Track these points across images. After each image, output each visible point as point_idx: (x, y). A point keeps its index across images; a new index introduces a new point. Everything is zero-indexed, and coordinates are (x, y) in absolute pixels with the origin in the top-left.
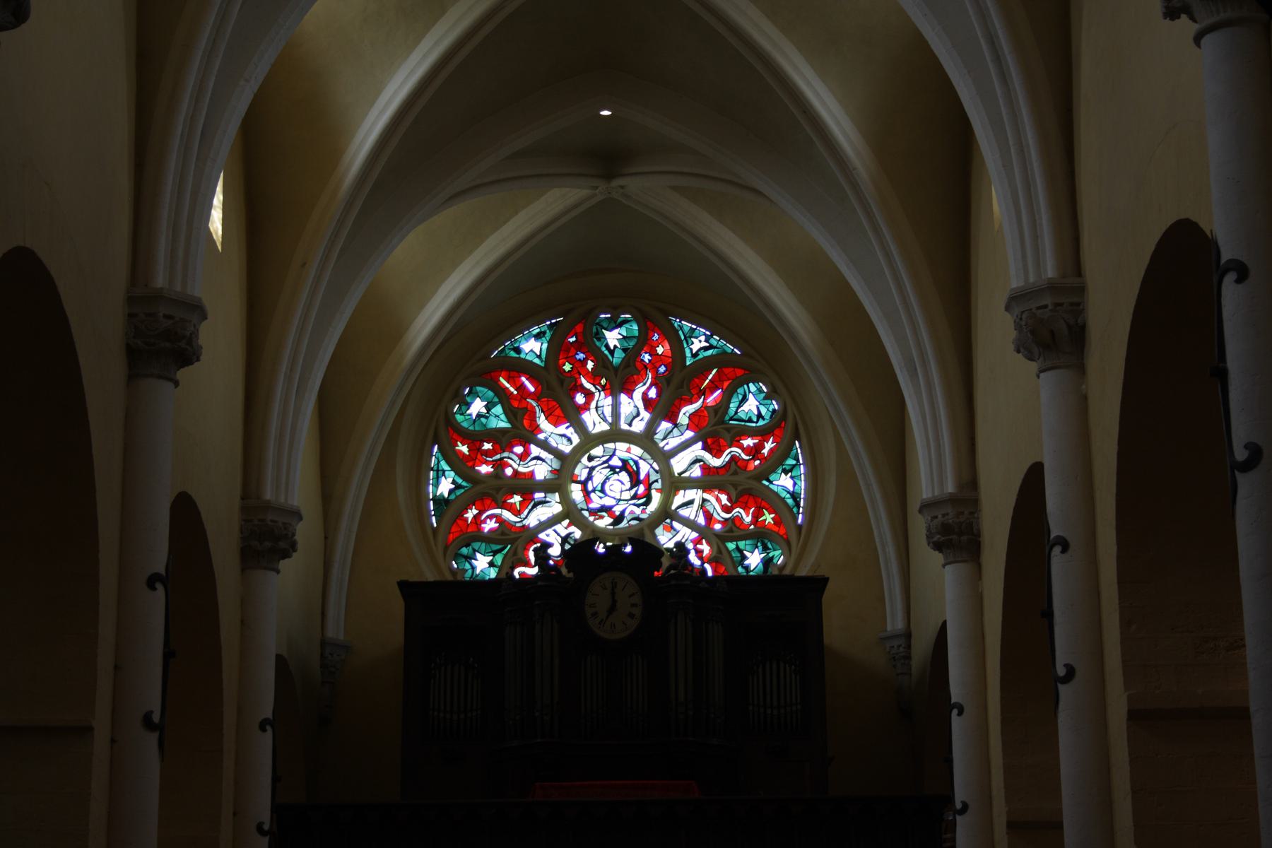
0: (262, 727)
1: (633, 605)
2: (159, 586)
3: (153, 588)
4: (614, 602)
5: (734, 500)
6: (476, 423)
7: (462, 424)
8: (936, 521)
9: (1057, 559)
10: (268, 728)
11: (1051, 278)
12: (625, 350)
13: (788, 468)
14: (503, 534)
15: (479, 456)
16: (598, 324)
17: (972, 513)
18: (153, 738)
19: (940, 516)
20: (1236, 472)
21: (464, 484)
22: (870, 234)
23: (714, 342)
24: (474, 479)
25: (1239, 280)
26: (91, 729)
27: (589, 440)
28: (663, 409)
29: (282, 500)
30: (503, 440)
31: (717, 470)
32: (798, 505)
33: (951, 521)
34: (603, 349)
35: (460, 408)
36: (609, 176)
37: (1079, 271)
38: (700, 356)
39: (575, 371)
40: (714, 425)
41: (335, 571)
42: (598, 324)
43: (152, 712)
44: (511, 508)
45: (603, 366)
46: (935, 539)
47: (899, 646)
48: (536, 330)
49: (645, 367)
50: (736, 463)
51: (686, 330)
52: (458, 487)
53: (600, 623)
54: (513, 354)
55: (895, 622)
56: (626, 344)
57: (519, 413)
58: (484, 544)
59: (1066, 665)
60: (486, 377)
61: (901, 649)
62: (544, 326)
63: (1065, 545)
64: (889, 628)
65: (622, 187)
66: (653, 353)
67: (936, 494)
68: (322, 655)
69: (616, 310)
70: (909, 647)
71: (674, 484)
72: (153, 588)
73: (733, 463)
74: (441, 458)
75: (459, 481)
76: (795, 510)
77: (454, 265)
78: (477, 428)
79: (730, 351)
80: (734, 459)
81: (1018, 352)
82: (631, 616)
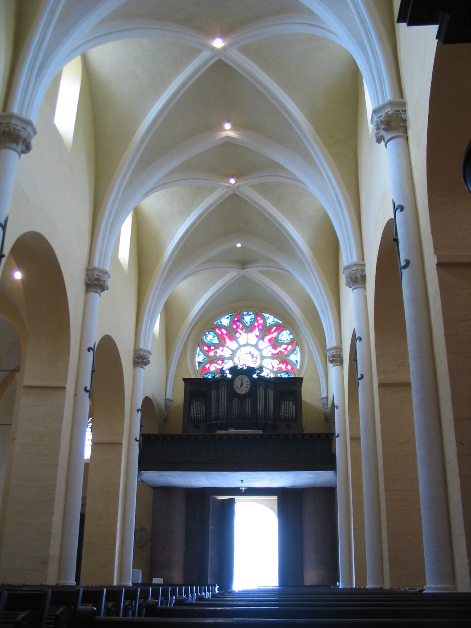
1: (248, 384)
4: (242, 384)
8: (330, 354)
12: (251, 322)
13: (295, 354)
14: (216, 371)
16: (243, 315)
17: (341, 352)
20: (402, 270)
21: (206, 358)
23: (275, 320)
25: (401, 211)
26: (64, 388)
27: (240, 346)
28: (261, 337)
30: (217, 346)
31: (275, 354)
32: (297, 364)
34: (245, 322)
36: (243, 269)
37: (363, 260)
40: (275, 342)
42: (243, 315)
44: (219, 364)
45: (244, 325)
46: (330, 359)
47: (325, 401)
48: (226, 317)
49: (256, 327)
51: (267, 316)
52: (205, 359)
54: (220, 323)
55: (324, 395)
56: (251, 321)
57: (221, 337)
58: (211, 374)
60: (213, 329)
61: (326, 402)
63: (360, 339)
64: (322, 396)
65: (247, 272)
66: (258, 322)
68: (165, 403)
69: (248, 311)
70: (328, 401)
73: (280, 352)
74: (200, 351)
75: (205, 357)
76: (297, 365)
79: (279, 322)
80: (280, 351)
81: (347, 286)
82: (247, 387)
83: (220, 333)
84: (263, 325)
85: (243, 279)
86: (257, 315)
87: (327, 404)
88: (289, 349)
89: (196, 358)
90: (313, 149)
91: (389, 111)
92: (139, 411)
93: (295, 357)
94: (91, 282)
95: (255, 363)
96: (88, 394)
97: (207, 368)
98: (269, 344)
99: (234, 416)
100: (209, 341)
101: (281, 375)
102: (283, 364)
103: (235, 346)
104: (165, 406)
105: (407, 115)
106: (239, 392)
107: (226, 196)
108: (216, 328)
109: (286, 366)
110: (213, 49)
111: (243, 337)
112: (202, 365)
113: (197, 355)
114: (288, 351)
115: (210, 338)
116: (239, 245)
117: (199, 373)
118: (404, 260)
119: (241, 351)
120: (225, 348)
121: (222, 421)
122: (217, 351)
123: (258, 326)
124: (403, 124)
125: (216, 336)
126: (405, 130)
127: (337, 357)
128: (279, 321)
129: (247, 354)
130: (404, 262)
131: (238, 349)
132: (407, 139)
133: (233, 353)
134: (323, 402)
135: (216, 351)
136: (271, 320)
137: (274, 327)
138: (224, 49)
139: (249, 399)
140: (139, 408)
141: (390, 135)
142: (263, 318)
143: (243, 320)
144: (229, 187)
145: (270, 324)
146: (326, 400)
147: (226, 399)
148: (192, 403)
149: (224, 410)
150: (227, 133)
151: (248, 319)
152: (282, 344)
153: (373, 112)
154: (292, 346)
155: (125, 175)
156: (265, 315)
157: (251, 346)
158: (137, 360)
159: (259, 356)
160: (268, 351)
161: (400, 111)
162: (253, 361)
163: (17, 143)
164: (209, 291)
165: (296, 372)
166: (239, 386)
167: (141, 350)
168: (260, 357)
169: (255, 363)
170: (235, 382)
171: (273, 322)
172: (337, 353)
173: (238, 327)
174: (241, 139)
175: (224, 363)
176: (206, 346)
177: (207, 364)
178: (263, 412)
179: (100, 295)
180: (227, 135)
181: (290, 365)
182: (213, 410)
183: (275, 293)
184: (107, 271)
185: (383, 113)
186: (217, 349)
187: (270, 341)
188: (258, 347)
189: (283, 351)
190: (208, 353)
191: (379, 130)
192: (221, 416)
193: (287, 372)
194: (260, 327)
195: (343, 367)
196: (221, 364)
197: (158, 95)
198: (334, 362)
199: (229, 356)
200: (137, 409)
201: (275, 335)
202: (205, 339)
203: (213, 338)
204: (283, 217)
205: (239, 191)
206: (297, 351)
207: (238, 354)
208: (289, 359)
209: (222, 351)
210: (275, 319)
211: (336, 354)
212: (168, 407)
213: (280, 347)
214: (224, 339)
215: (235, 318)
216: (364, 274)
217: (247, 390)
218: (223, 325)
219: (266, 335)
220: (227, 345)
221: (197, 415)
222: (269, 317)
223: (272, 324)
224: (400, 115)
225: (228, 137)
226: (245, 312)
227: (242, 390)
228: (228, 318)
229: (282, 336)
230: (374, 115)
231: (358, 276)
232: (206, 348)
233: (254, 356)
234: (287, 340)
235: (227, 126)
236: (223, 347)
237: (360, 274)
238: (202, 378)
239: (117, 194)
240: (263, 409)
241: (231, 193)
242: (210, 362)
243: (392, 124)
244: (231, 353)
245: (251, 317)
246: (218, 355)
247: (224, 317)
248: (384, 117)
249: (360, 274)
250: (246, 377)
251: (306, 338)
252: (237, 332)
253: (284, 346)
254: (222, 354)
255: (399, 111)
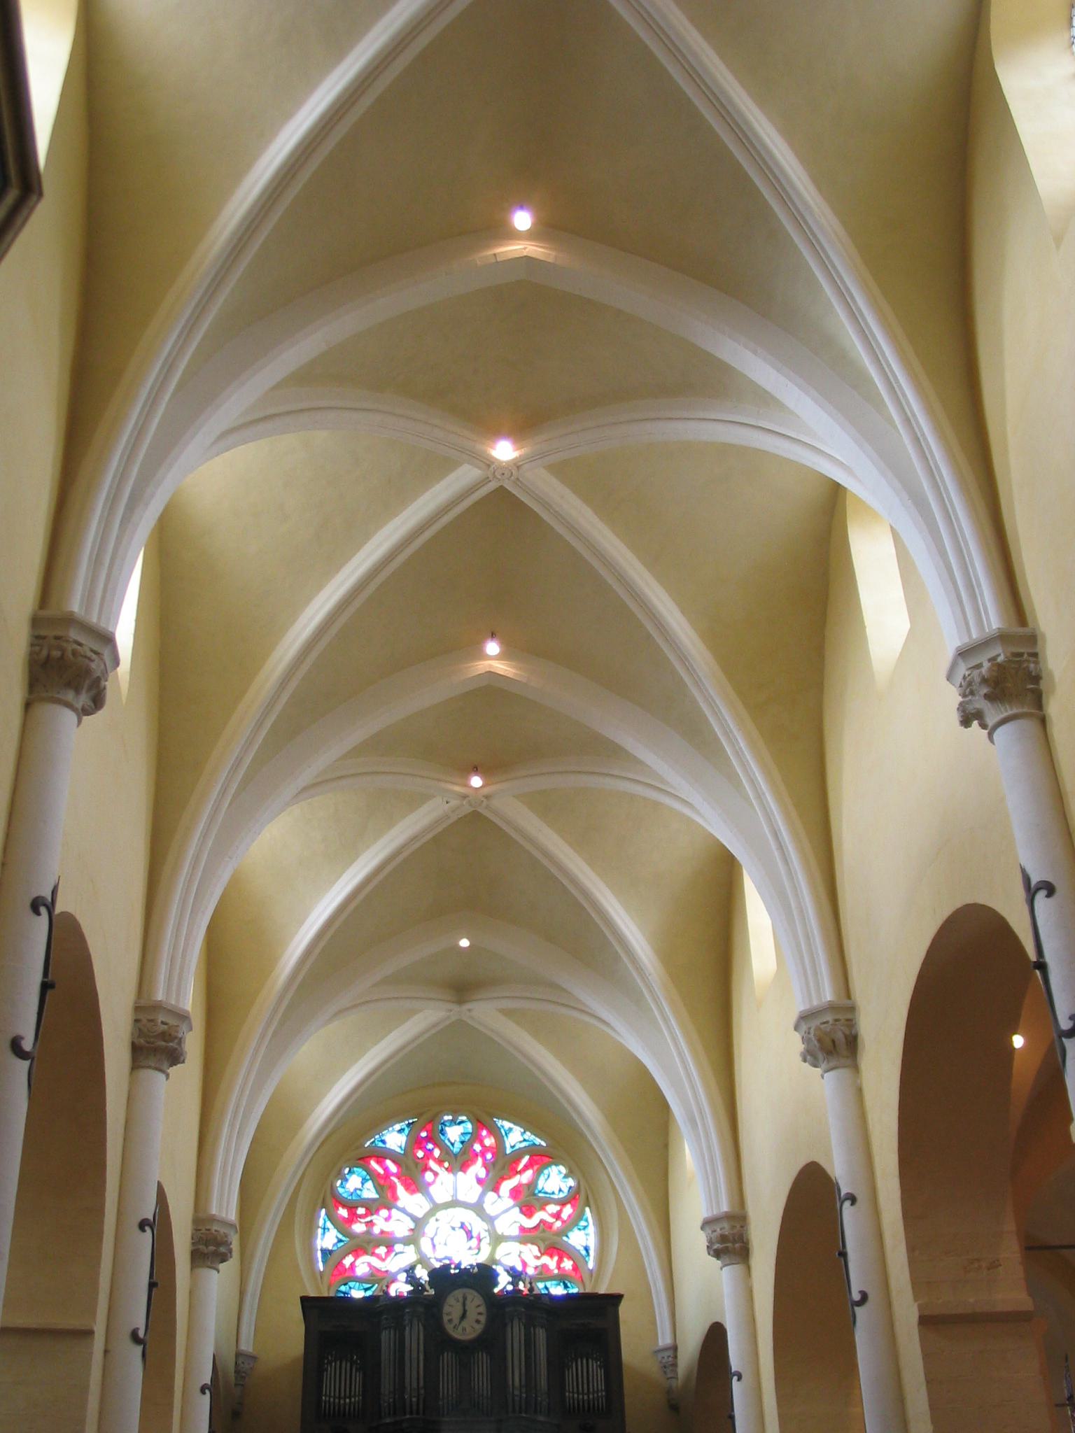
0: (203, 1391)
1: (480, 1314)
2: (147, 1228)
3: (143, 1230)
5: (542, 1252)
6: (353, 1195)
7: (343, 1195)
8: (715, 1234)
9: (848, 1213)
10: (207, 1392)
11: (830, 1001)
12: (462, 1142)
13: (582, 1228)
14: (372, 1275)
15: (355, 1219)
17: (742, 1227)
18: (139, 1349)
19: (718, 1230)
20: (1063, 1039)
21: (344, 1239)
22: (661, 1022)
23: (527, 1138)
24: (351, 1236)
27: (436, 1208)
29: (224, 1215)
30: (372, 1207)
31: (530, 1230)
32: (588, 1254)
33: (727, 1233)
34: (447, 1142)
35: (342, 1183)
36: (461, 1002)
38: (517, 1147)
39: (426, 1157)
41: (248, 1299)
42: (442, 1124)
43: (138, 1329)
44: (379, 1257)
45: (446, 1151)
47: (669, 1357)
48: (398, 1127)
49: (476, 1155)
50: (544, 1224)
51: (506, 1128)
53: (454, 1327)
54: (381, 1144)
55: (665, 1340)
56: (463, 1138)
57: (383, 1183)
58: (358, 1284)
59: (860, 1292)
60: (363, 1160)
61: (670, 1359)
62: (403, 1125)
63: (853, 1199)
64: (660, 1344)
67: (715, 1213)
69: (455, 1113)
70: (676, 1357)
71: (497, 1239)
72: (143, 1230)
73: (542, 1225)
74: (327, 1219)
75: (340, 1236)
76: (587, 1259)
77: (345, 1070)
78: (354, 1198)
79: (537, 1143)
80: (542, 1221)
81: (805, 1060)
82: (478, 1321)
83: (381, 1171)
84: (495, 1150)
85: (459, 1028)
86: (480, 1124)
87: (675, 1365)
88: (565, 1215)
89: (316, 1238)
90: (716, 713)
91: (999, 655)
92: (207, 1392)
93: (582, 1238)
94: (148, 1043)
95: (477, 1254)
96: (139, 1349)
97: (347, 1266)
98: (511, 1202)
99: (445, 1401)
100: (352, 1194)
101: (546, 1288)
102: (551, 1257)
103: (421, 1207)
104: (235, 1372)
105: (1041, 665)
106: (457, 1335)
107: (454, 818)
108: (370, 1157)
109: (560, 1261)
110: (489, 463)
111: (443, 1183)
112: (333, 1260)
113: (320, 1231)
114: (563, 1222)
115: (355, 1184)
116: (464, 943)
117: (326, 1279)
118: (1068, 1017)
119: (437, 1220)
120: (394, 1211)
121: (415, 1416)
122: (374, 1221)
123: (483, 1154)
124: (1032, 686)
125: (371, 1179)
126: (1038, 700)
127: (734, 1239)
128: (538, 1141)
129: (453, 1229)
130: (1069, 1021)
131: (431, 1213)
132: (1043, 721)
133: (416, 1225)
134: (664, 1361)
135: (371, 1221)
136: (516, 1137)
137: (525, 1155)
138: (517, 465)
139: (484, 1355)
140: (206, 1382)
141: (1002, 709)
142: (495, 1132)
143: (442, 1137)
144: (464, 797)
145: (514, 1149)
146: (670, 1353)
147: (422, 1357)
148: (326, 1366)
149: (418, 1386)
150: (490, 666)
151: (454, 1134)
152: (548, 1201)
153: (959, 654)
154: (573, 1206)
155: (238, 762)
156: (500, 1123)
157: (466, 1208)
158: (202, 1247)
159: (487, 1233)
160: (511, 1220)
161: (1026, 656)
162: (470, 1248)
163: (77, 691)
164: (361, 1062)
165: (586, 1277)
166: (456, 1321)
167: (213, 1219)
168: (488, 1238)
169: (477, 1254)
170: (446, 1309)
171: (521, 1142)
172: (735, 1231)
173: (429, 1154)
174: (524, 680)
175: (394, 1253)
176: (344, 1206)
177: (347, 1255)
178: (524, 1390)
179: (168, 1076)
180: (488, 670)
181: (570, 1258)
182: (386, 1386)
183: (539, 1068)
184: (188, 1012)
185: (984, 659)
186: (372, 1215)
187: (515, 1193)
188: (484, 1210)
189: (551, 1220)
190: (350, 1226)
191: (970, 697)
192: (411, 1401)
193: (562, 1278)
194: (489, 1156)
195: (749, 1268)
196: (384, 1257)
197: (333, 564)
198: (725, 1254)
199: (407, 1233)
200: (201, 1385)
201: (526, 1177)
202: (342, 1186)
203: (363, 1184)
204: (592, 875)
205: (487, 807)
206: (587, 1220)
207: (430, 1229)
208: (567, 1242)
209: (388, 1219)
210: (528, 1133)
211: (732, 1232)
212: (244, 1375)
213: (543, 1209)
214: (393, 1188)
215: (421, 1131)
216: (853, 1033)
217: (479, 1328)
218: (389, 1149)
219: (503, 1179)
220: (400, 1204)
221: (340, 1398)
222: (510, 1129)
223: (520, 1149)
224: (1025, 665)
225: (491, 674)
226: (448, 1115)
227: (464, 1329)
228: (401, 1131)
229: (546, 1180)
230: (960, 661)
231: (839, 1036)
232: (343, 1212)
233: (475, 1234)
234: (560, 1190)
235: (492, 648)
236: (389, 1209)
237: (844, 1033)
238: (332, 1297)
239: (216, 809)
240: (523, 1383)
241: (467, 809)
242: (356, 1250)
243: (1009, 685)
244: (412, 1225)
245: (464, 1128)
246: (376, 1230)
247: (390, 1129)
248: (990, 669)
249: (842, 1030)
250: (476, 1294)
251: (319, 1148)
252: (427, 1168)
253: (553, 1208)
254: (388, 1227)
255: (1021, 655)
